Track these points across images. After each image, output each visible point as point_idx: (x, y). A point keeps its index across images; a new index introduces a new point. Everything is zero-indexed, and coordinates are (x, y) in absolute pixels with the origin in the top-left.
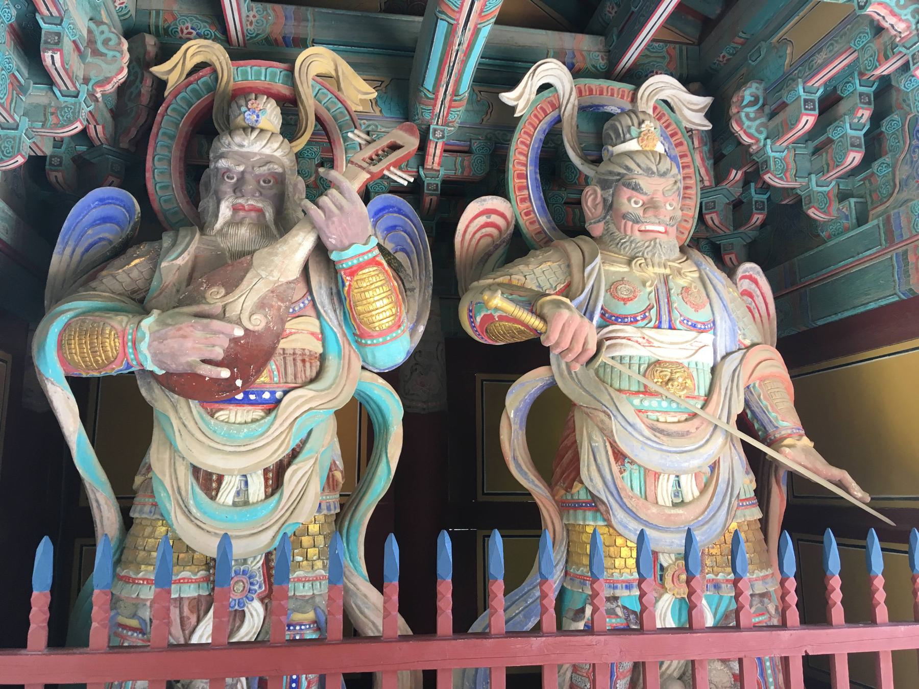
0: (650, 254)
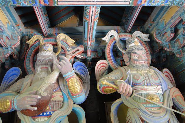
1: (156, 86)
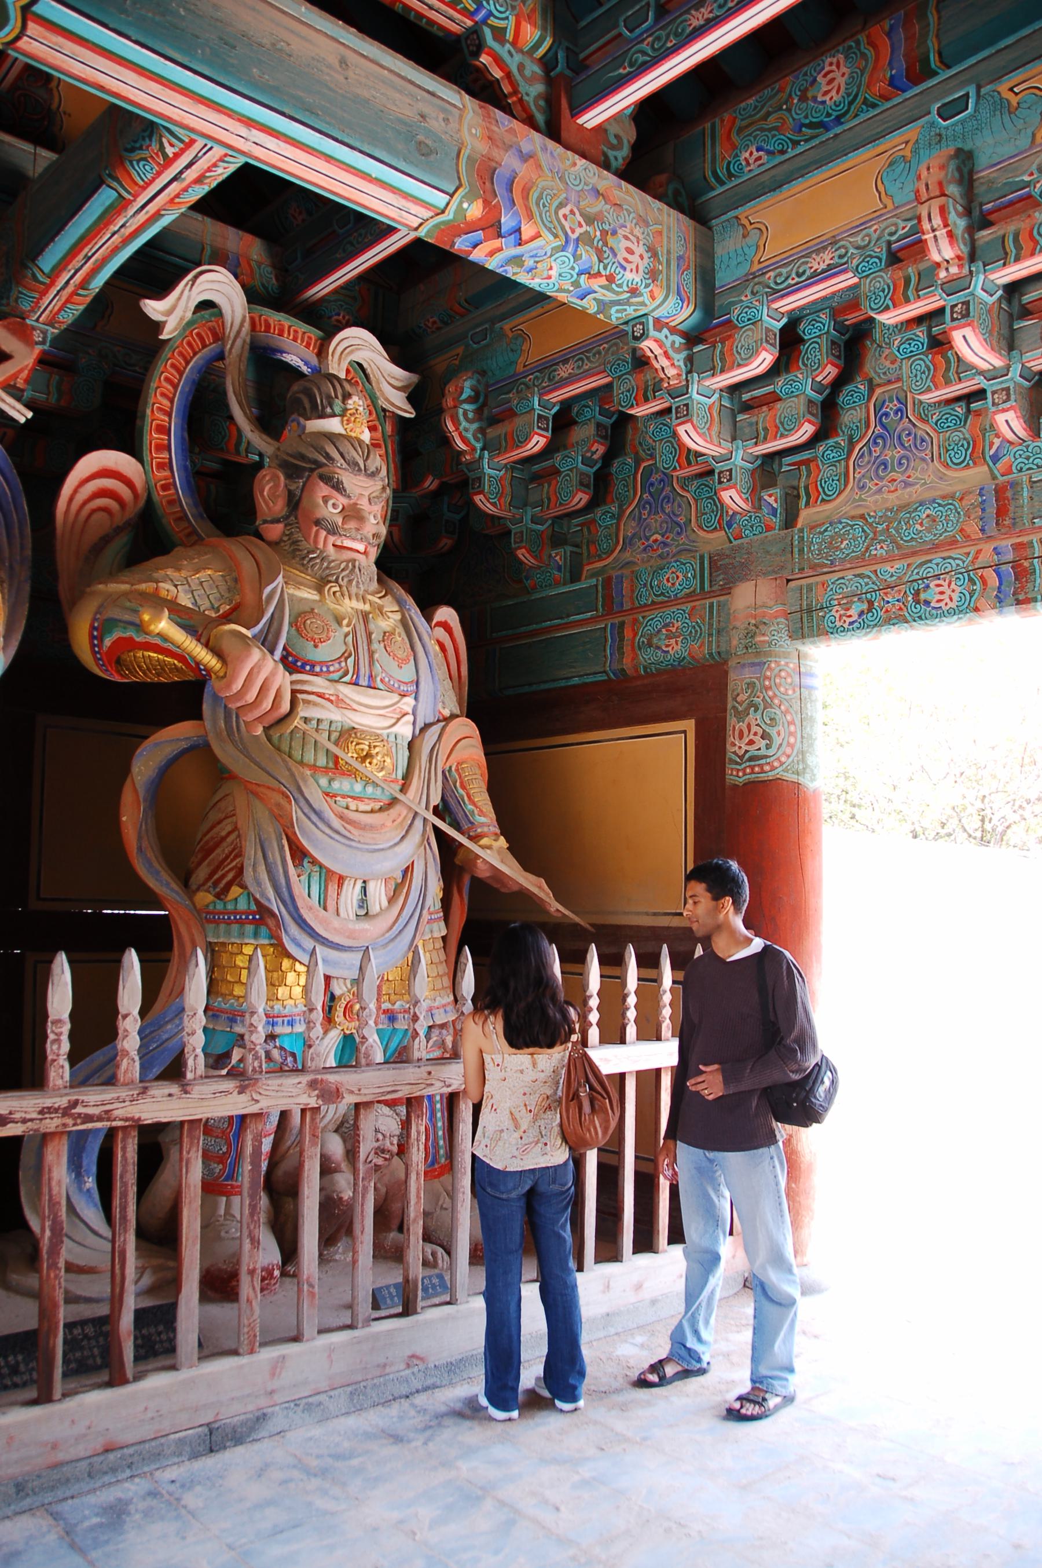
0: (346, 580)
1: (396, 697)
